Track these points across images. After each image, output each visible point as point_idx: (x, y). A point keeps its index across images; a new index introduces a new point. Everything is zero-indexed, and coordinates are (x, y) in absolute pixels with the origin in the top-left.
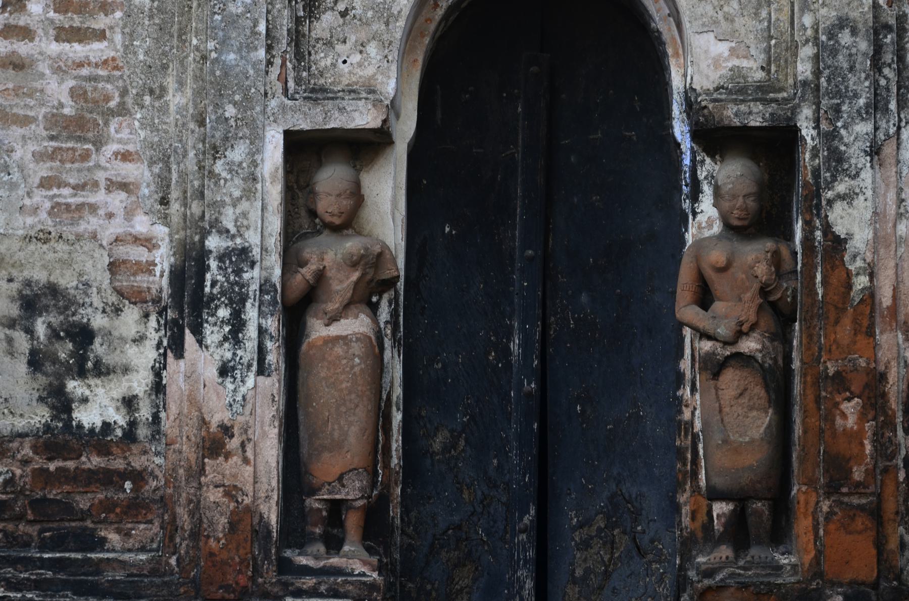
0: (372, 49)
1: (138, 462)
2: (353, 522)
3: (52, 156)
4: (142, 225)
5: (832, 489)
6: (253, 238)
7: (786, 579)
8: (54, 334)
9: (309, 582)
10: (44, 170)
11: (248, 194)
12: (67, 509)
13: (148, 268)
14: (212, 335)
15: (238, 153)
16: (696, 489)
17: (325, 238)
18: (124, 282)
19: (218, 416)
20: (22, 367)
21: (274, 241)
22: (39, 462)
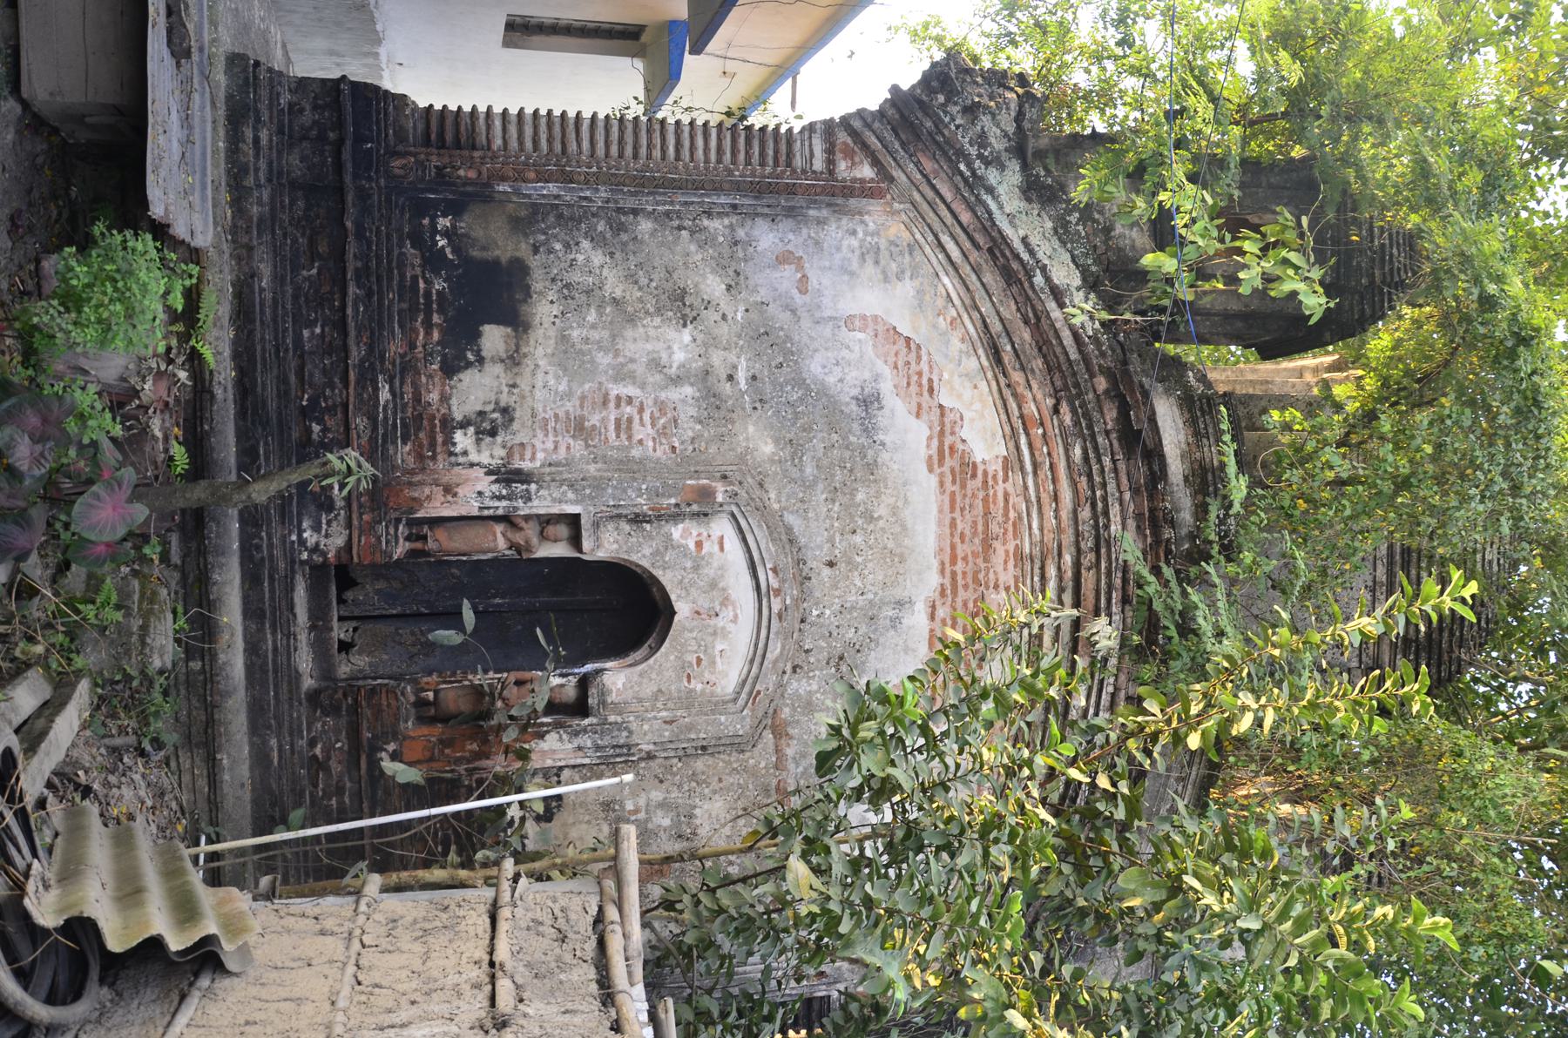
0: (615, 546)
1: (440, 457)
2: (418, 545)
3: (568, 418)
4: (540, 456)
5: (441, 741)
6: (536, 503)
7: (402, 725)
8: (493, 421)
9: (392, 531)
10: (562, 414)
11: (554, 500)
12: (419, 429)
13: (522, 459)
14: (495, 488)
15: (570, 495)
16: (438, 683)
17: (538, 528)
18: (516, 449)
19: (460, 491)
20: (479, 408)
21: (535, 511)
22: (438, 416)
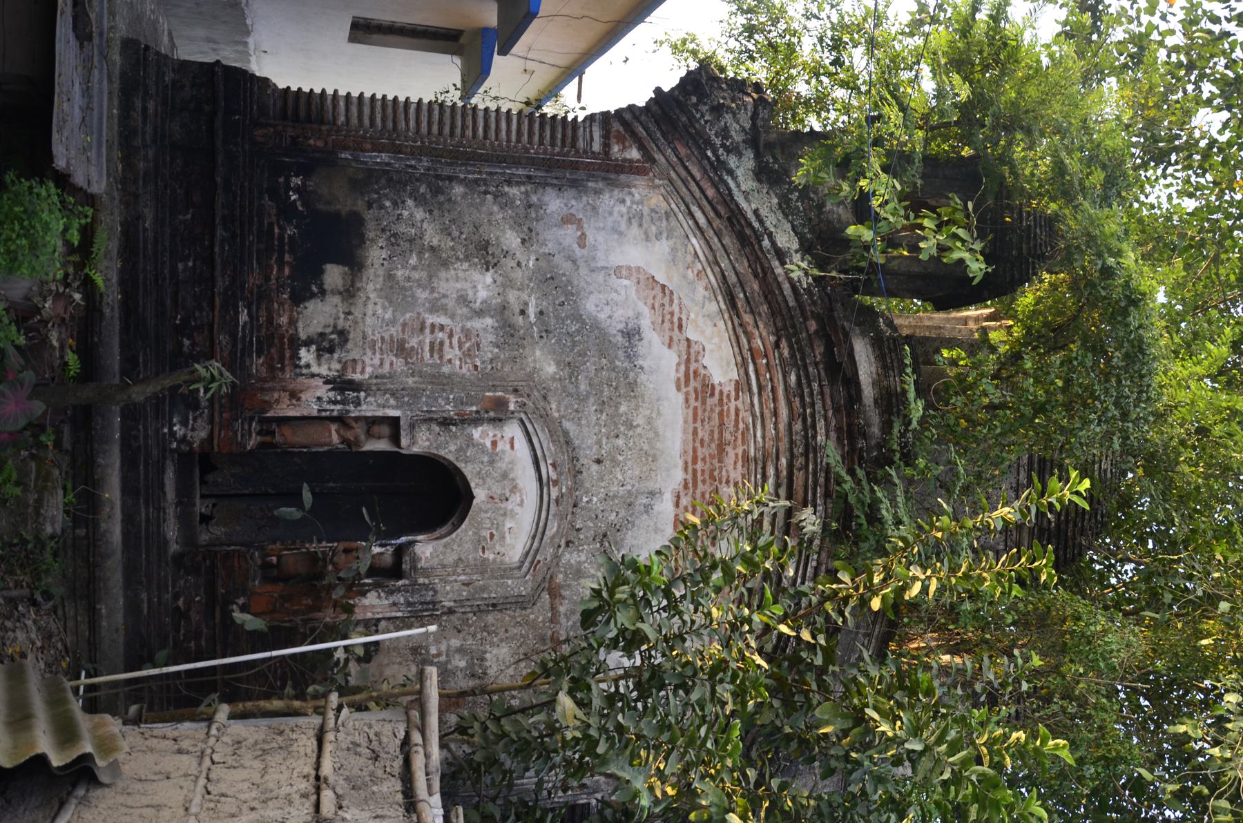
1: (287, 369)
2: (268, 439)
4: (369, 370)
6: (364, 407)
7: (250, 584)
8: (332, 341)
9: (246, 427)
11: (379, 405)
12: (271, 345)
13: (354, 371)
14: (331, 394)
15: (392, 402)
16: (281, 550)
17: (365, 428)
18: (349, 364)
19: (303, 396)
20: (320, 330)
21: (363, 414)
22: (287, 336)
